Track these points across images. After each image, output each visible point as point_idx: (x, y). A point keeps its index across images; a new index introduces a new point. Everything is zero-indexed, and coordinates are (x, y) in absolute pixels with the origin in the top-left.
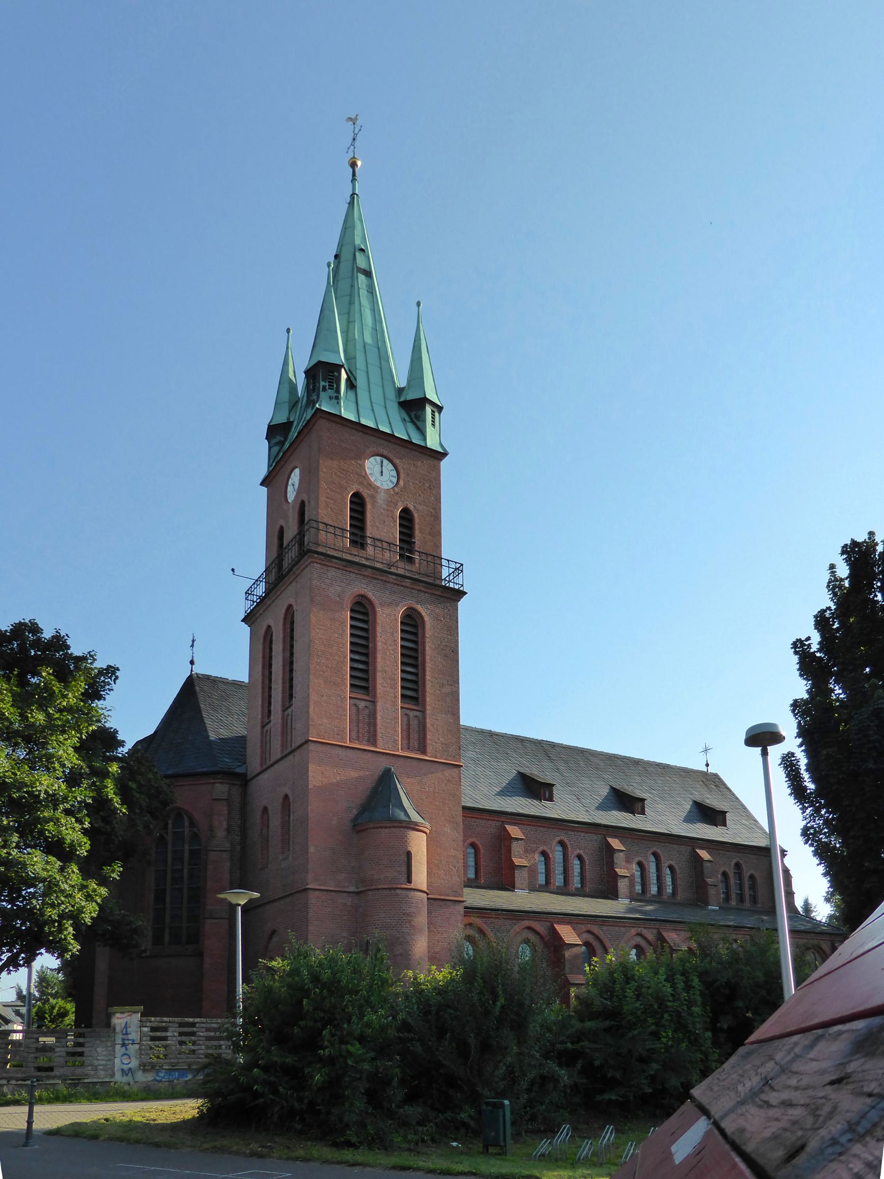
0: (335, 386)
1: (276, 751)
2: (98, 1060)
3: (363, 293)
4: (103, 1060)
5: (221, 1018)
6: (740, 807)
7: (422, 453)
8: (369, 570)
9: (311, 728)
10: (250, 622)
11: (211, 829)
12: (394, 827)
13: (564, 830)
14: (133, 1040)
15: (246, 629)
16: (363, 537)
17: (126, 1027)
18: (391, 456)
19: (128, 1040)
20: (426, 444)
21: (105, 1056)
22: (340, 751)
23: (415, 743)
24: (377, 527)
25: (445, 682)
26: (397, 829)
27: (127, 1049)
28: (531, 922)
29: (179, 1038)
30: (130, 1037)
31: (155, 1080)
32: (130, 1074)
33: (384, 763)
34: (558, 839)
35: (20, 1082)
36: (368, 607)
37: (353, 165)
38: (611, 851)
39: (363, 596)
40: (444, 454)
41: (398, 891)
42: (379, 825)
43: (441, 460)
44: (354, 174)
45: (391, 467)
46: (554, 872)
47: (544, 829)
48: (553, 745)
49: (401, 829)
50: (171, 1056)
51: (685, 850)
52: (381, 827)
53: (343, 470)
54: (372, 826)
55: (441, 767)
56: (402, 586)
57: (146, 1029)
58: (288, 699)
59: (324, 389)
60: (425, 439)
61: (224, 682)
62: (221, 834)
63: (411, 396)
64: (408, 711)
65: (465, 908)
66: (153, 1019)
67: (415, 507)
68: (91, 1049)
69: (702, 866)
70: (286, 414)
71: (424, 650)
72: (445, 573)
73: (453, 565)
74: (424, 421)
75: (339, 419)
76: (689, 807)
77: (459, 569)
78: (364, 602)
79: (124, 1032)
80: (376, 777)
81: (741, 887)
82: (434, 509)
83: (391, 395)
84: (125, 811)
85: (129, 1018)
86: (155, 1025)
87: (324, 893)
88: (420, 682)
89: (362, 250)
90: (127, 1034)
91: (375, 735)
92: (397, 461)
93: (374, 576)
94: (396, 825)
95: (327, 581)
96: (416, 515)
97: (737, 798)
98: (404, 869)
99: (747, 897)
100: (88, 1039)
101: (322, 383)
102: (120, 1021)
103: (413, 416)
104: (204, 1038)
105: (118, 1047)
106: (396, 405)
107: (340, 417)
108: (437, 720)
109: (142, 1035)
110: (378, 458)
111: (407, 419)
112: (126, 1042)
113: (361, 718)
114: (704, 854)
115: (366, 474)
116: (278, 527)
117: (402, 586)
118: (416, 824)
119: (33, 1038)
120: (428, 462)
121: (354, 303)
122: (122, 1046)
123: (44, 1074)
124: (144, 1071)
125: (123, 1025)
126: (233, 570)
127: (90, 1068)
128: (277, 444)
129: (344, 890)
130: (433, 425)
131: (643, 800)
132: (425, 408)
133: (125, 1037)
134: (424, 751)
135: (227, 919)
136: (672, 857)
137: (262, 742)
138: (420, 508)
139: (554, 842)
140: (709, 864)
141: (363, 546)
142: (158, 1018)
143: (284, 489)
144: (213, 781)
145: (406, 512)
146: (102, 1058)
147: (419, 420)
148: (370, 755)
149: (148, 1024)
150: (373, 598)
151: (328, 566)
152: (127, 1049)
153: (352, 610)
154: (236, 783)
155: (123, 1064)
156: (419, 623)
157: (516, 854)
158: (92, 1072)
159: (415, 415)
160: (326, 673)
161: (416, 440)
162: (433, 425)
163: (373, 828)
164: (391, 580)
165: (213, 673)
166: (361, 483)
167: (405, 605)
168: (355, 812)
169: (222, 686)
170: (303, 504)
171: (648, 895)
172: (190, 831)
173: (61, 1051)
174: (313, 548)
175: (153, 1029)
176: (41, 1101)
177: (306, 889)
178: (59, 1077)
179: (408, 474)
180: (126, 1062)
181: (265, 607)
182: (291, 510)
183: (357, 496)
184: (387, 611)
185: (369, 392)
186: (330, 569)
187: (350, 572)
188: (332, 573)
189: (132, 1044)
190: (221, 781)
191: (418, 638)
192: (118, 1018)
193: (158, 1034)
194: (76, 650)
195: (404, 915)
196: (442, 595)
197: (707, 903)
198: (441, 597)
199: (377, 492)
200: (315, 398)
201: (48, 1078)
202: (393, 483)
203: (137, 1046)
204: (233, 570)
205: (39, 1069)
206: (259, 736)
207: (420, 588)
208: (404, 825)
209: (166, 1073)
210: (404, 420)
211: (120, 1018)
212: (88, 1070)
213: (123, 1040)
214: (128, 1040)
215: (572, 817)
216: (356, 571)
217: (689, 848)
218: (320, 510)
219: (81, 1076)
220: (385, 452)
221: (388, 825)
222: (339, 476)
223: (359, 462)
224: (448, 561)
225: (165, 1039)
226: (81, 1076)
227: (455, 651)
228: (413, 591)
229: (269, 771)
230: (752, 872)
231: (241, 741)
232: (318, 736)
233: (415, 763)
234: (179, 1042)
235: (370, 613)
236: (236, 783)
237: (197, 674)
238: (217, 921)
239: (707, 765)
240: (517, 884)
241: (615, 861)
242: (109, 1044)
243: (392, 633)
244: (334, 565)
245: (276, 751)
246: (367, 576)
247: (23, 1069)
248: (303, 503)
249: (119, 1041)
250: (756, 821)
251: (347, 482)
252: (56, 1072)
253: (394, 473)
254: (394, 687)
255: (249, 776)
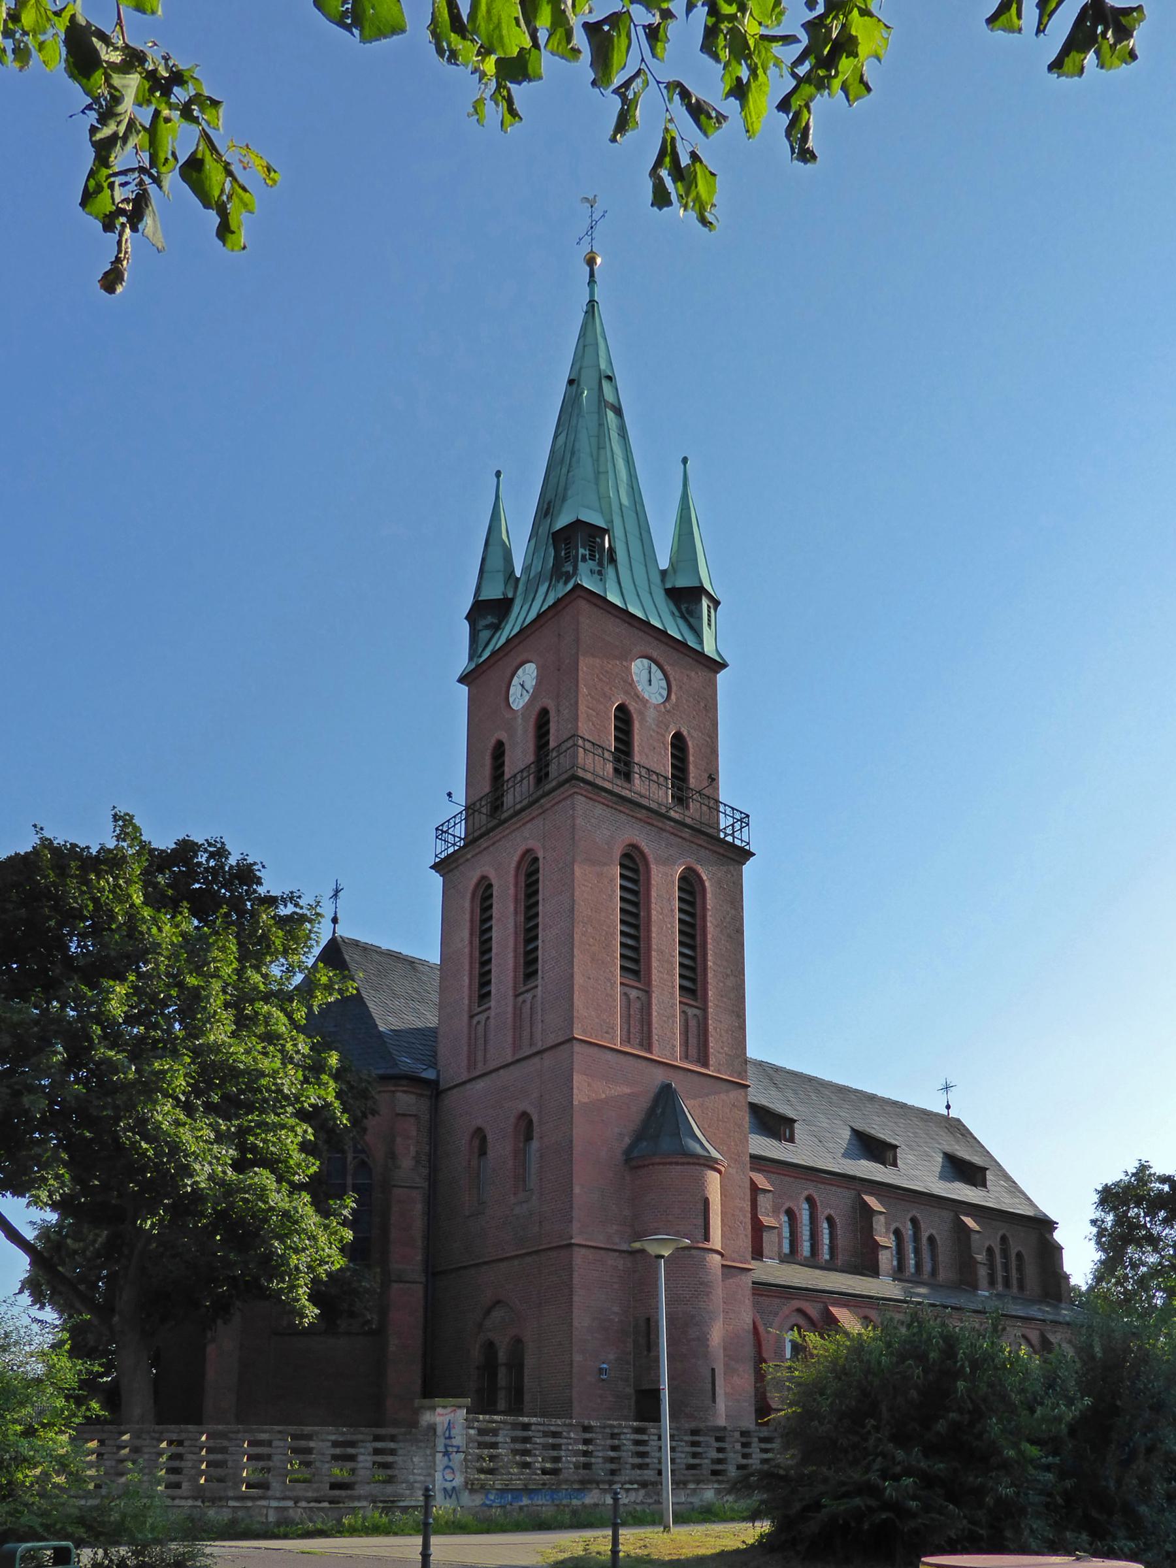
0: (597, 556)
1: (501, 1049)
2: (414, 1474)
3: (614, 435)
4: (420, 1475)
5: (536, 1416)
6: (993, 1163)
7: (697, 661)
8: (644, 811)
9: (575, 1020)
10: (446, 870)
11: (392, 1155)
12: (688, 1163)
13: (813, 1181)
14: (458, 1447)
15: (437, 880)
16: (628, 764)
17: (450, 1426)
18: (661, 661)
19: (452, 1446)
20: (703, 648)
21: (422, 1468)
22: (609, 1056)
23: (693, 1051)
24: (647, 756)
25: (729, 972)
26: (692, 1167)
27: (450, 1460)
28: (802, 1302)
29: (512, 1446)
30: (455, 1442)
31: (484, 1505)
32: (454, 1496)
33: (660, 1076)
34: (806, 1193)
35: (312, 1504)
36: (638, 861)
37: (591, 262)
38: (868, 1212)
39: (635, 847)
40: (724, 665)
41: (694, 1252)
42: (669, 1160)
43: (718, 672)
44: (592, 275)
45: (659, 675)
46: (801, 1237)
47: (792, 1179)
48: (777, 1069)
49: (697, 1167)
50: (503, 1471)
51: (947, 1215)
52: (671, 1163)
53: (607, 672)
54: (658, 1160)
55: (724, 1086)
56: (681, 837)
57: (472, 1432)
58: (521, 979)
59: (584, 559)
60: (701, 642)
61: (377, 950)
62: (406, 1162)
63: (682, 582)
64: (687, 1007)
65: (754, 1283)
66: (481, 1417)
67: (689, 732)
68: (405, 1458)
69: (969, 1238)
70: (501, 588)
71: (704, 927)
72: (724, 822)
73: (738, 816)
74: (700, 618)
75: (600, 601)
76: (941, 1160)
77: (745, 820)
78: (635, 854)
79: (447, 1435)
80: (651, 1095)
81: (1006, 1267)
82: (710, 737)
83: (656, 578)
84: (345, 1122)
85: (452, 1415)
86: (483, 1426)
87: (592, 1250)
88: (699, 970)
89: (609, 378)
90: (450, 1438)
91: (650, 1037)
92: (667, 668)
93: (649, 821)
94: (691, 1160)
95: (593, 820)
96: (690, 744)
97: (988, 1152)
98: (700, 1221)
99: (1014, 1282)
100: (401, 1445)
101: (581, 551)
102: (442, 1418)
103: (684, 610)
104: (540, 1447)
105: (439, 1456)
106: (662, 593)
107: (605, 599)
108: (721, 1022)
109: (470, 1439)
110: (646, 661)
111: (677, 613)
112: (450, 1449)
113: (632, 1012)
114: (969, 1222)
115: (633, 680)
116: (493, 741)
117: (681, 837)
118: (716, 1161)
119: (329, 1441)
120: (698, 676)
121: (604, 448)
122: (444, 1456)
123: (343, 1493)
124: (472, 1491)
125: (446, 1425)
126: (449, 795)
127: (404, 1485)
128: (487, 627)
129: (615, 1247)
130: (709, 625)
131: (896, 1147)
132: (701, 600)
133: (448, 1442)
134: (705, 1064)
135: (421, 1283)
136: (935, 1226)
137: (470, 1038)
138: (695, 734)
139: (802, 1198)
140: (977, 1236)
141: (628, 777)
142: (487, 1417)
143: (504, 689)
144: (393, 1089)
145: (678, 738)
146: (420, 1471)
147: (692, 616)
148: (644, 1063)
149: (476, 1424)
150: (646, 850)
151: (595, 800)
152: (450, 1460)
153: (622, 865)
154: (425, 1093)
155: (446, 1480)
156: (697, 889)
157: (763, 1210)
158: (408, 1492)
159: (687, 609)
160: (593, 948)
161: (692, 643)
162: (709, 625)
163: (659, 1164)
164: (668, 828)
165: (364, 938)
166: (626, 693)
167: (681, 865)
168: (627, 1140)
169: (376, 957)
170: (544, 714)
171: (907, 1274)
172: (354, 1158)
173: (366, 1461)
174: (581, 773)
175: (481, 1432)
176: (624, 1524)
177: (570, 1245)
178: (365, 1498)
179: (681, 687)
180: (449, 1477)
181: (477, 850)
182: (520, 721)
183: (622, 708)
184: (662, 869)
185: (631, 570)
186: (596, 804)
187: (621, 811)
188: (599, 810)
189: (457, 1452)
190: (405, 1089)
191: (695, 909)
192: (439, 1415)
193: (488, 1439)
194: (269, 886)
195: (701, 1284)
196: (725, 853)
197: (975, 1287)
198: (723, 855)
199: (645, 706)
200: (570, 569)
201: (352, 1498)
202: (663, 697)
203: (462, 1456)
204: (449, 795)
205: (334, 1486)
206: (465, 1030)
207: (700, 842)
208: (702, 1161)
209: (497, 1494)
210: (673, 614)
211: (442, 1415)
212: (401, 1488)
213: (446, 1446)
214: (452, 1446)
215: (820, 1164)
216: (627, 811)
217: (952, 1214)
218: (580, 724)
219: (394, 1496)
220: (655, 655)
221: (681, 1160)
222: (601, 680)
223: (625, 663)
224: (733, 809)
225: (494, 1445)
226: (394, 1496)
227: (740, 931)
228: (692, 845)
229: (487, 1079)
230: (1020, 1248)
231: (428, 1036)
232: (584, 1032)
233: (696, 1078)
234: (512, 1451)
235: (641, 868)
236: (425, 1093)
237: (341, 937)
238: (407, 1285)
239: (948, 1107)
240: (766, 1252)
241: (874, 1226)
242: (428, 1452)
243: (669, 899)
244: (603, 800)
245: (501, 1049)
246: (641, 820)
247: (315, 1486)
248: (544, 714)
249: (441, 1448)
250: (1014, 1182)
251: (611, 689)
252: (360, 1490)
253: (664, 684)
254: (670, 973)
255: (443, 1086)
